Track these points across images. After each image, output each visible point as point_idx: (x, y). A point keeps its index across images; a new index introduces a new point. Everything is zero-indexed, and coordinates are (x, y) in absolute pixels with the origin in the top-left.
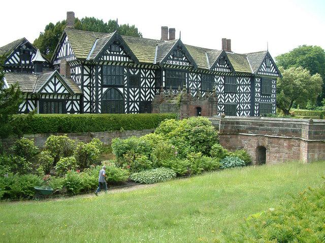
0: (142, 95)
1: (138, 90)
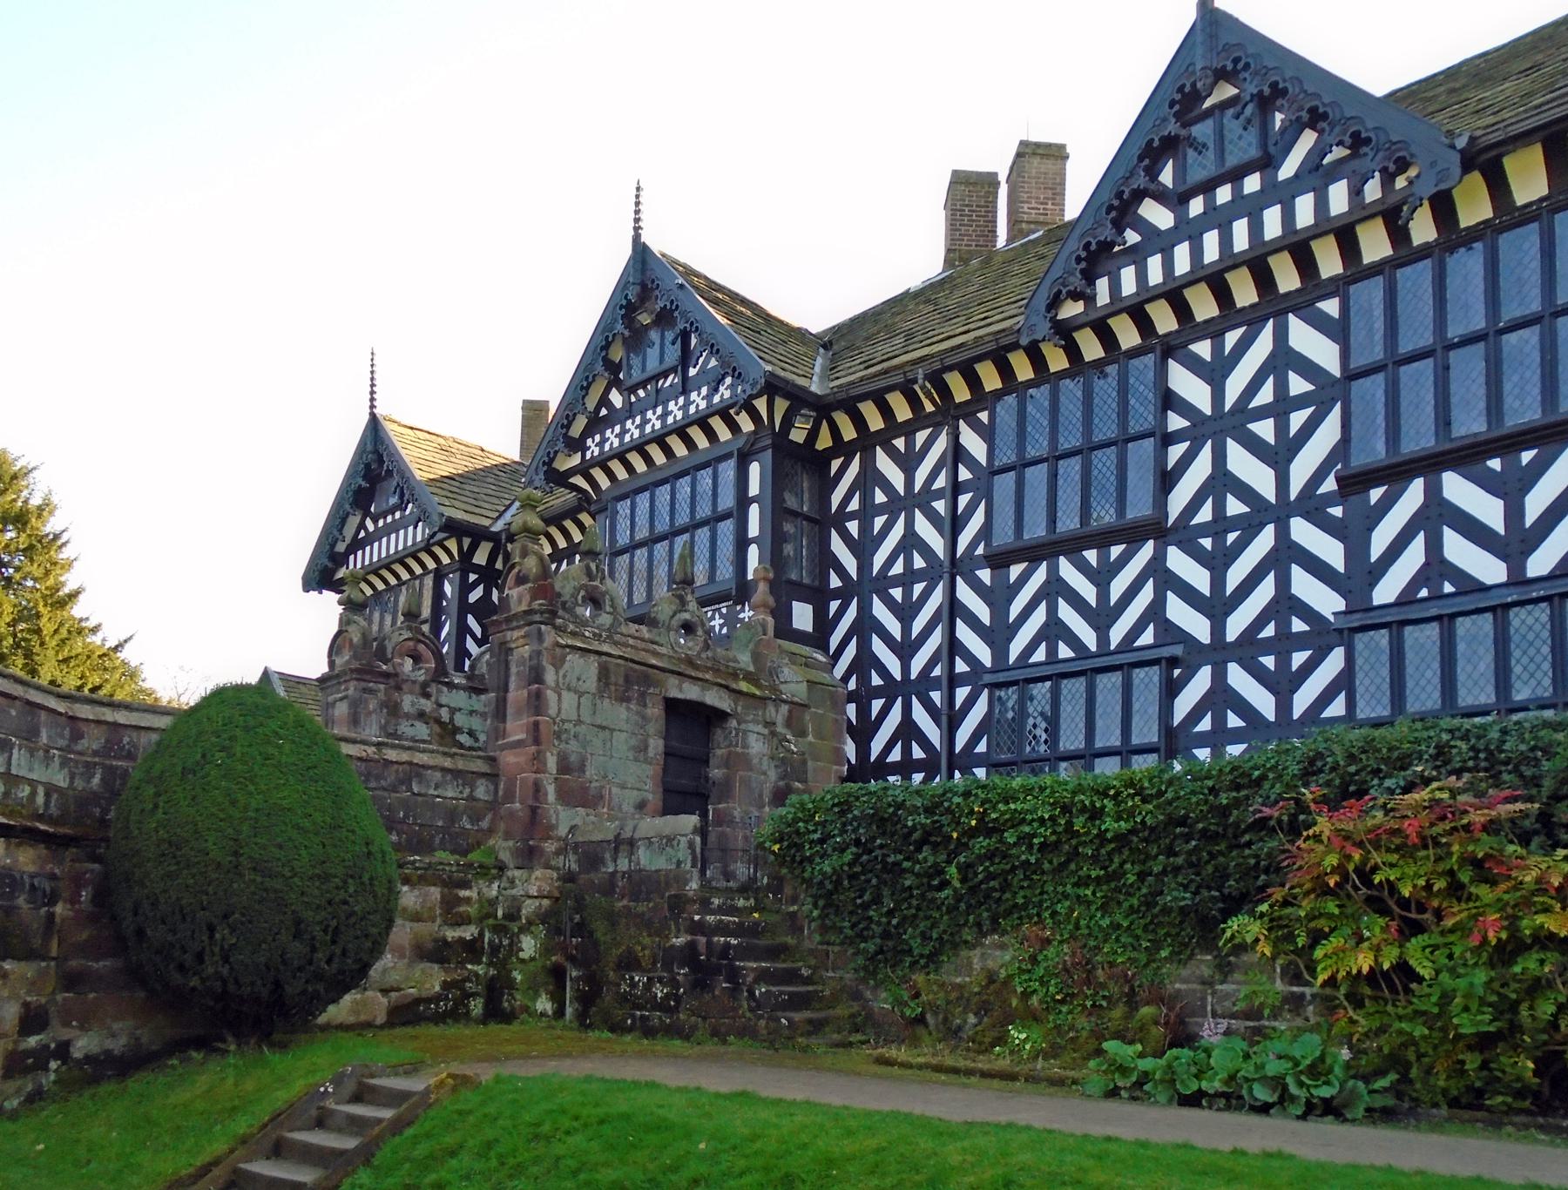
0: (983, 612)
1: (1016, 648)
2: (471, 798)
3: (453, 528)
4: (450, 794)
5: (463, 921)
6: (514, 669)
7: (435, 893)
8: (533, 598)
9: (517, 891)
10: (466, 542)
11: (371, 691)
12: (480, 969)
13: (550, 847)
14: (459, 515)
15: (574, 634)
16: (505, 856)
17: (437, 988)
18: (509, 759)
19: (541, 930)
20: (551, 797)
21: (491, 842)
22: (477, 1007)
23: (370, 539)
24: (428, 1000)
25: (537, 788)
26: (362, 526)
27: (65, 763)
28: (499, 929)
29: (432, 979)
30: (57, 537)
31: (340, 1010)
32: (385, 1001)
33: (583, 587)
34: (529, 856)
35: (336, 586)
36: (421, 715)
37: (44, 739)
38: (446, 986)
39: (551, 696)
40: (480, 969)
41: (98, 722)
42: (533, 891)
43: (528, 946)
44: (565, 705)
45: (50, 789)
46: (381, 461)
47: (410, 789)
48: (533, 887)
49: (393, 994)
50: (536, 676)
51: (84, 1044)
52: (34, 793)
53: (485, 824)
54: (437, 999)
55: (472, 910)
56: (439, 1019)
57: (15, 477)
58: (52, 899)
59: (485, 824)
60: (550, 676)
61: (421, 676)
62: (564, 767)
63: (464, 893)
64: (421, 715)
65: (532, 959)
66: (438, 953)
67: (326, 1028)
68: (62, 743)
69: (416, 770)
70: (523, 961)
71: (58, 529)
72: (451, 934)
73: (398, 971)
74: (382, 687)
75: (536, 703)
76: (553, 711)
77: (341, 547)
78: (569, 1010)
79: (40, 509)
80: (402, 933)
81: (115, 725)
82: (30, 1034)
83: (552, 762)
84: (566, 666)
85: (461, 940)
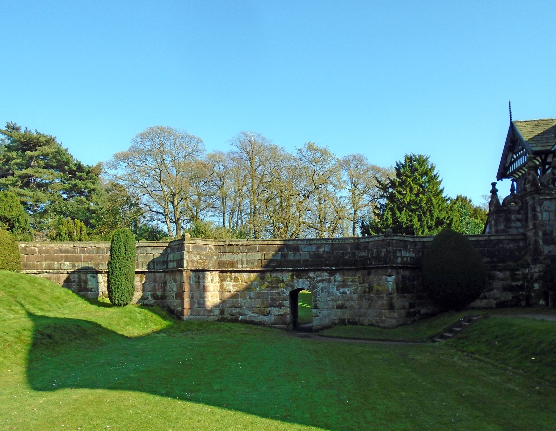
2: (518, 246)
3: (537, 154)
4: (511, 246)
5: (518, 280)
6: (529, 208)
7: (508, 273)
8: (531, 187)
9: (533, 271)
10: (543, 156)
11: (501, 216)
12: (524, 293)
13: (541, 258)
14: (538, 149)
15: (548, 194)
16: (529, 261)
17: (511, 298)
18: (530, 234)
19: (541, 282)
20: (541, 243)
21: (525, 258)
22: (523, 303)
23: (515, 160)
24: (508, 301)
25: (536, 242)
26: (513, 157)
27: (413, 252)
28: (528, 282)
29: (509, 296)
30: (435, 176)
31: (478, 303)
32: (495, 302)
33: (552, 178)
34: (536, 261)
35: (507, 177)
36: (518, 220)
37: (409, 247)
38: (513, 297)
39: (539, 215)
40: (524, 293)
41: (420, 242)
42: (537, 270)
43: (536, 286)
44: (544, 216)
45: (411, 258)
46: (515, 136)
47: (498, 246)
48: (536, 269)
49: (498, 300)
50: (534, 209)
51: (423, 311)
52: (407, 259)
53: (523, 253)
54: (510, 301)
55: (520, 277)
56: (511, 306)
57: (423, 162)
58: (413, 281)
59: (523, 253)
60: (538, 209)
61: (517, 208)
62: (545, 234)
63: (518, 272)
64: (518, 220)
65: (538, 290)
66: (510, 289)
67: (473, 308)
68: (412, 247)
69: (501, 241)
70: (535, 290)
71: (435, 173)
72: (514, 284)
73: (498, 293)
74: (503, 214)
75: (535, 217)
76: (540, 219)
77: (507, 165)
78: (550, 304)
79: (430, 169)
80: (498, 284)
81: (423, 242)
82: (412, 308)
83: (540, 233)
84: (544, 205)
85: (517, 286)
